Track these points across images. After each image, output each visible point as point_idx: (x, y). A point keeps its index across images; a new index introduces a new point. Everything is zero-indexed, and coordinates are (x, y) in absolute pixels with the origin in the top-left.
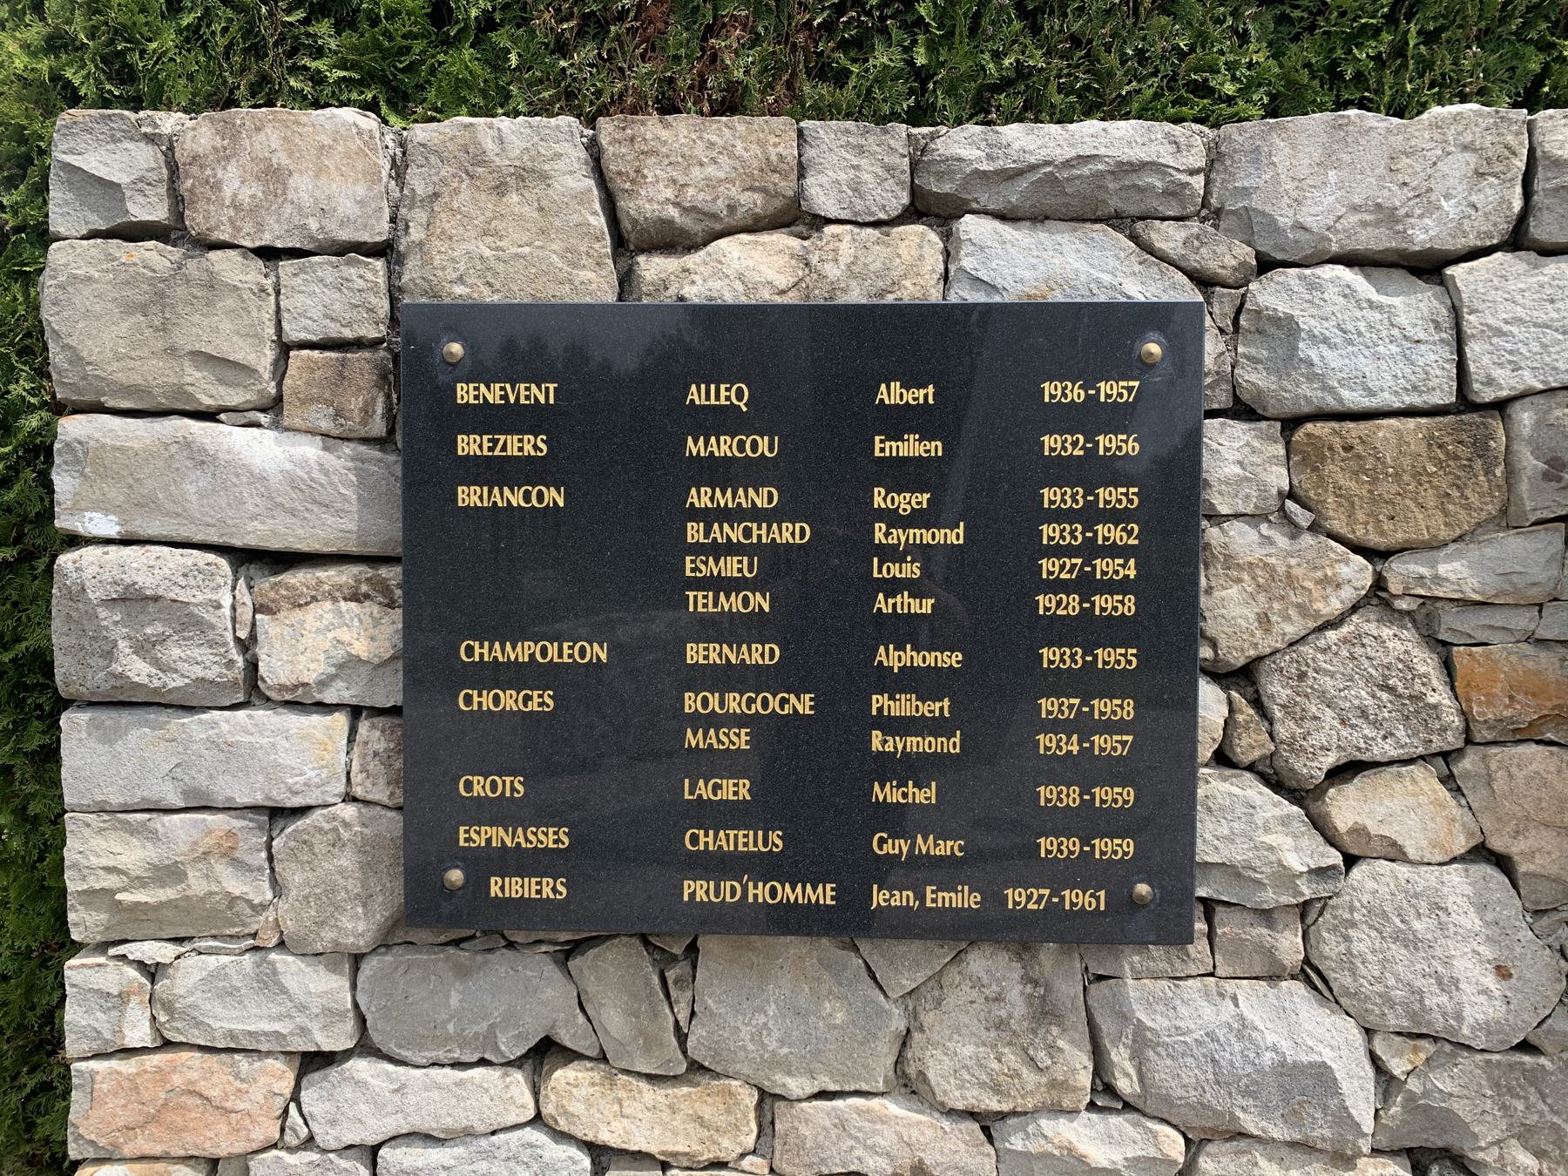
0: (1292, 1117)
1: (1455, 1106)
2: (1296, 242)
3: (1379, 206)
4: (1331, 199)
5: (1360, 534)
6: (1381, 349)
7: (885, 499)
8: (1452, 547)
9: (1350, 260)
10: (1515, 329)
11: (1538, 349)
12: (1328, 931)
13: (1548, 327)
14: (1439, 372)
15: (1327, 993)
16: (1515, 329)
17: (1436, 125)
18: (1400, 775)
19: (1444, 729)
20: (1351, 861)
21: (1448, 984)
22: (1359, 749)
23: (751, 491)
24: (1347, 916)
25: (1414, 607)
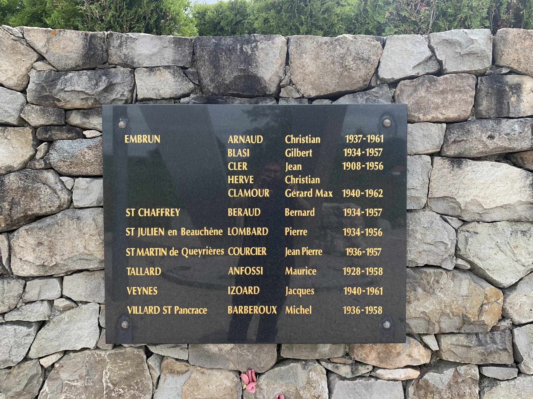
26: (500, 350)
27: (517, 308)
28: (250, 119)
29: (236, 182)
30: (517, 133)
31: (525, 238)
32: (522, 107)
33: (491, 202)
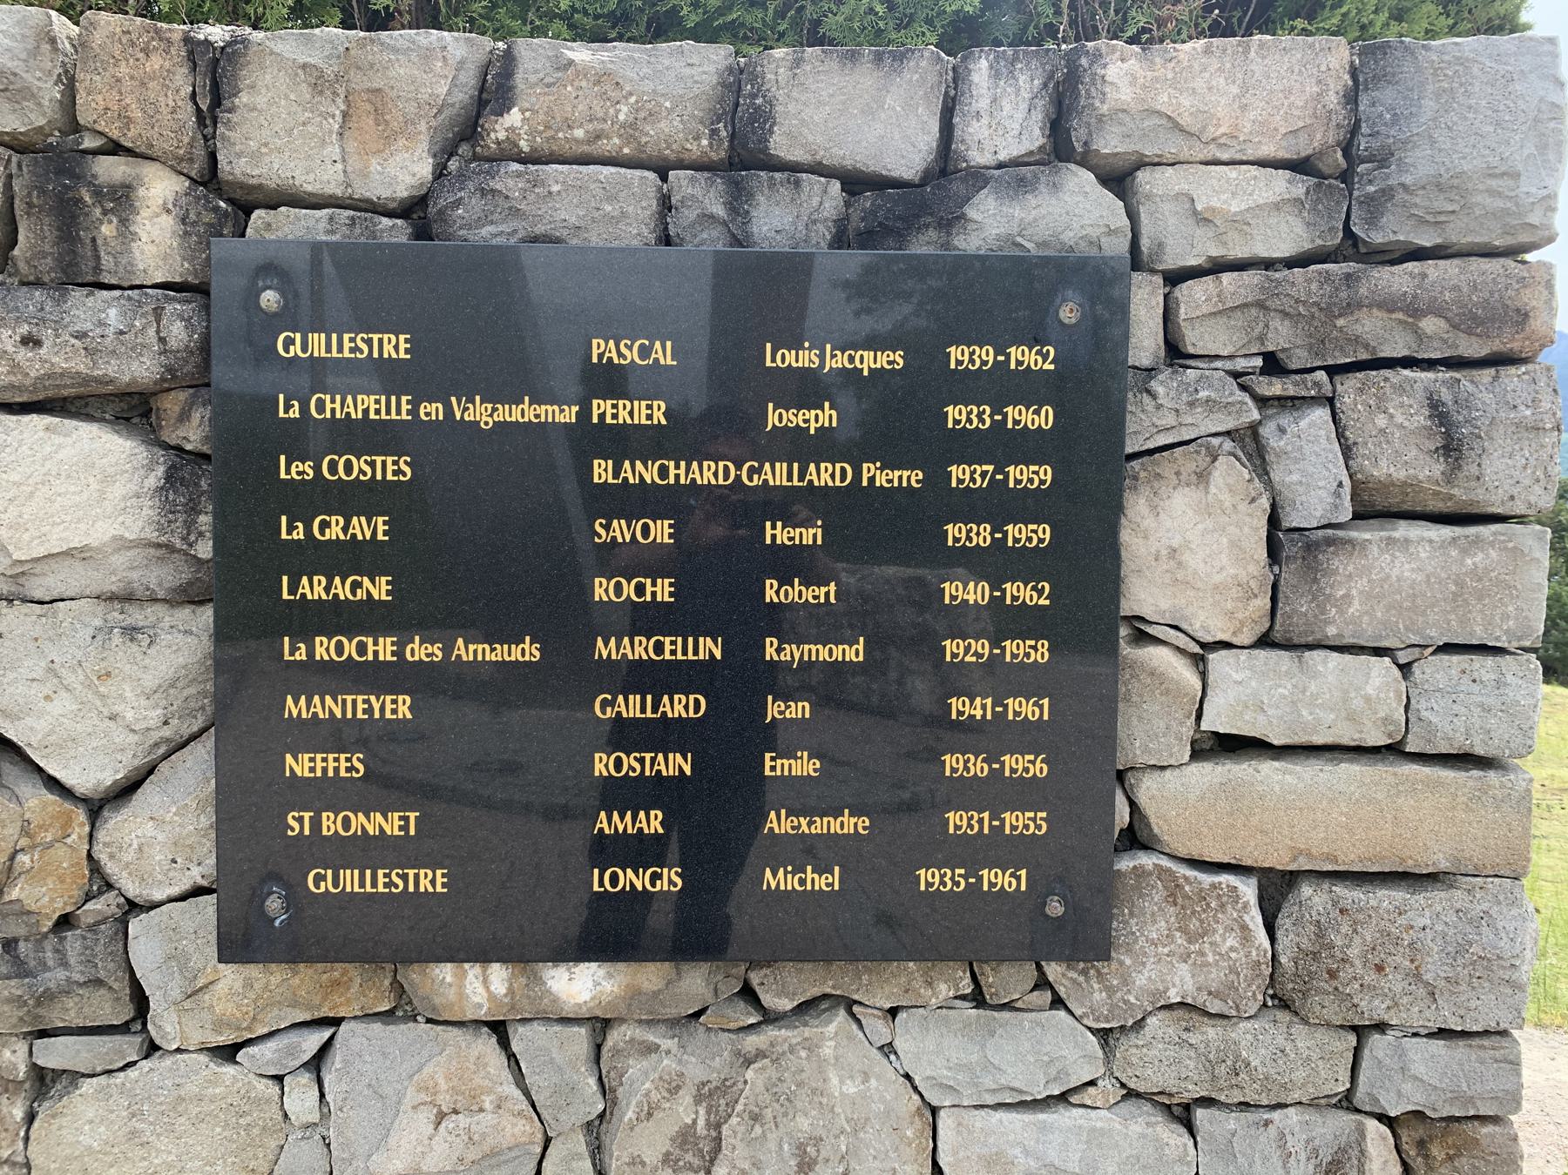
7: (777, 593)
26: (80, 985)
27: (129, 856)
28: (855, 306)
30: (110, 331)
31: (134, 648)
32: (137, 254)
33: (33, 539)
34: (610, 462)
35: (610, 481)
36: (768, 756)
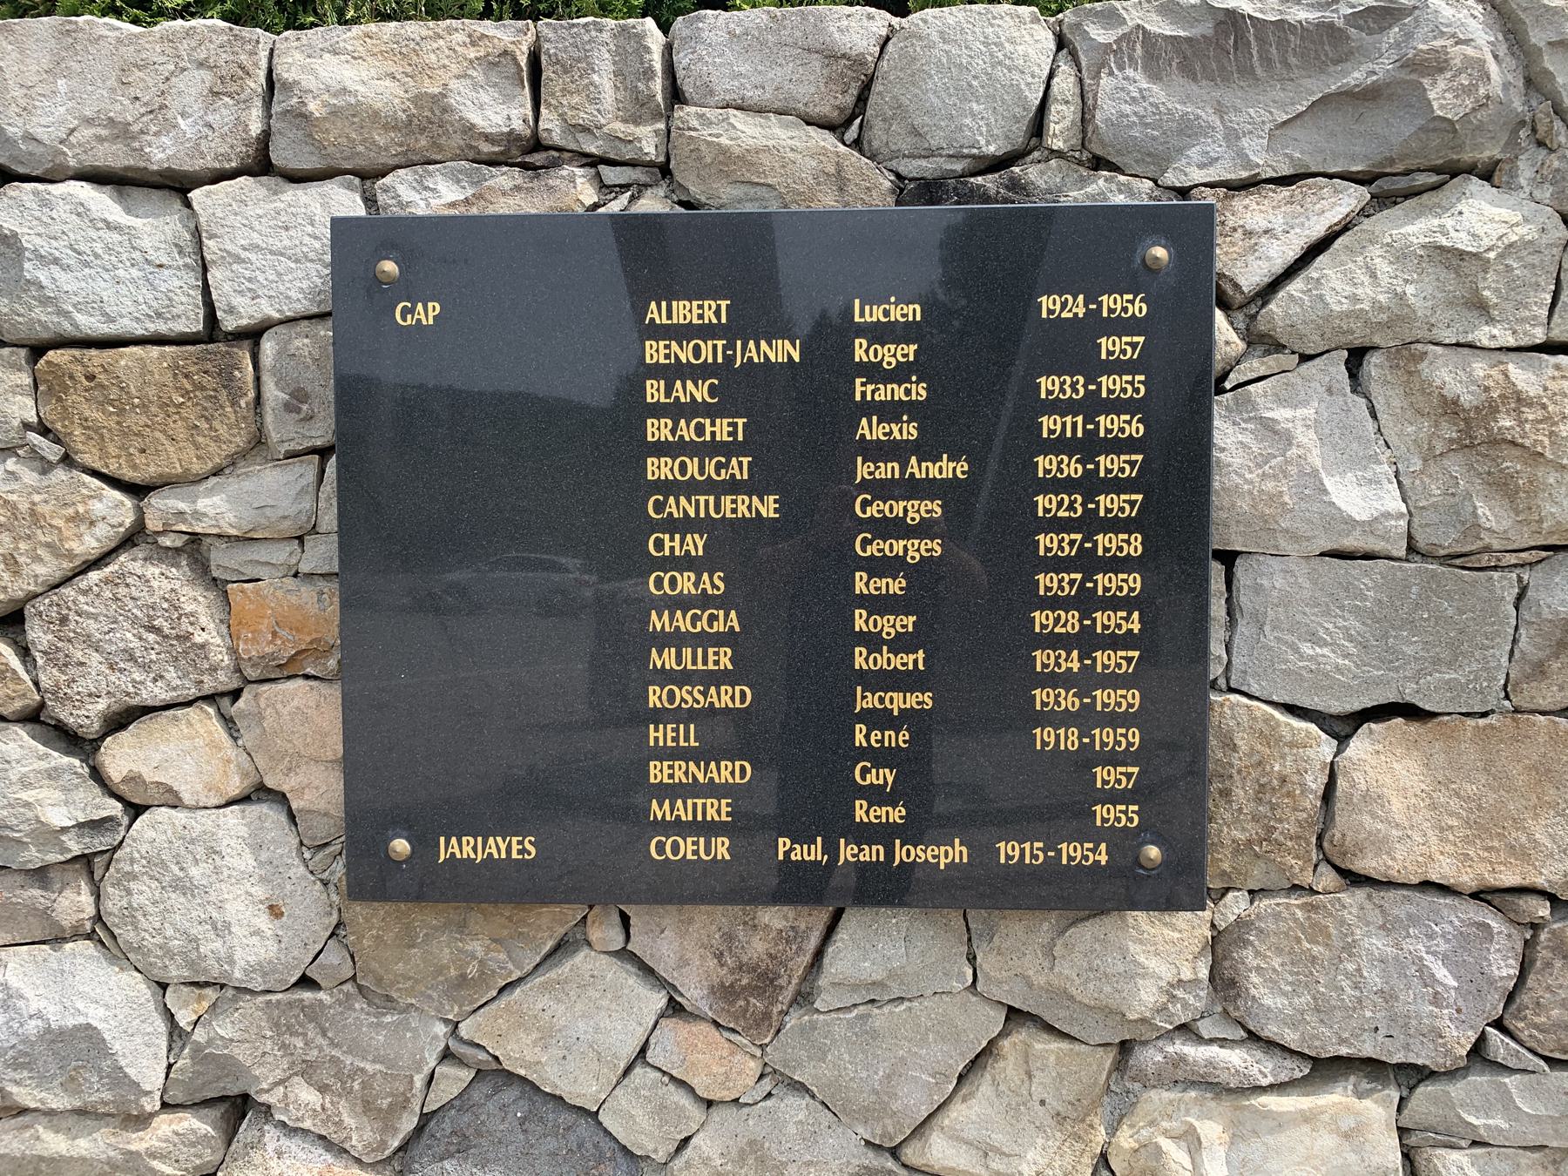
0: (71, 1084)
1: (236, 1051)
2: (31, 154)
3: (111, 120)
4: (62, 109)
5: (112, 468)
6: (121, 273)
8: (213, 480)
9: (97, 177)
10: (253, 257)
11: (273, 277)
12: (113, 885)
13: (282, 254)
14: (184, 299)
15: (115, 951)
16: (253, 257)
17: (168, 39)
18: (176, 719)
19: (213, 669)
20: (136, 810)
21: (221, 929)
22: (128, 694)
23: (689, 384)
24: (128, 868)
25: (179, 544)
29: (670, 743)
34: (662, 383)
35: (663, 400)
36: (858, 381)
